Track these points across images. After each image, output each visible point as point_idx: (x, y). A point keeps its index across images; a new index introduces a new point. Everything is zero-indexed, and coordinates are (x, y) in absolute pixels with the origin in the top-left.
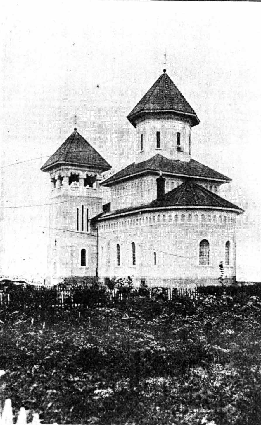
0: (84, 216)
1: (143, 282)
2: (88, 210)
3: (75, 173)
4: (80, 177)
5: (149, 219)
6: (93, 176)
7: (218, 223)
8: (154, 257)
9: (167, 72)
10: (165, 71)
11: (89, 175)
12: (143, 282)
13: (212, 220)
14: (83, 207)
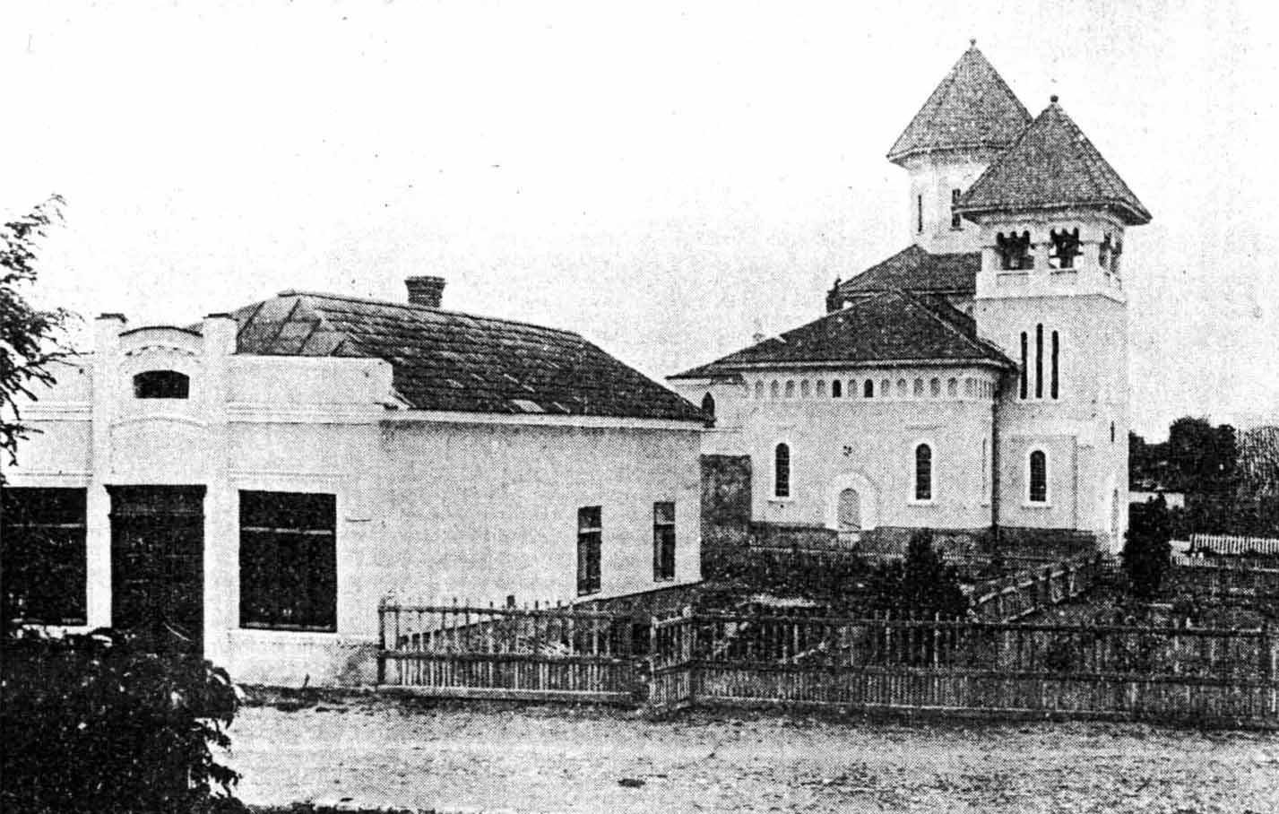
0: (337, 302)
1: (1081, 254)
2: (1055, 335)
3: (1014, 234)
4: (1033, 240)
5: (767, 392)
6: (1070, 231)
7: (910, 397)
8: (925, 211)
9: (1060, 103)
10: (1054, 99)
11: (1058, 231)
12: (1081, 254)
13: (813, 392)
14: (1040, 328)
